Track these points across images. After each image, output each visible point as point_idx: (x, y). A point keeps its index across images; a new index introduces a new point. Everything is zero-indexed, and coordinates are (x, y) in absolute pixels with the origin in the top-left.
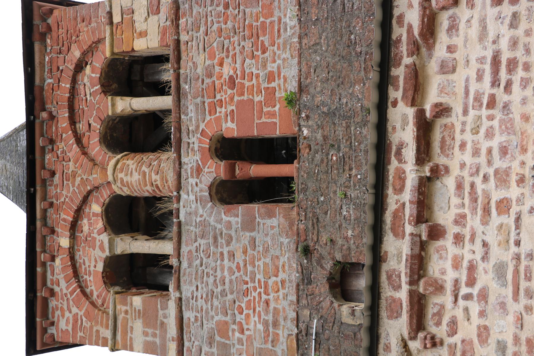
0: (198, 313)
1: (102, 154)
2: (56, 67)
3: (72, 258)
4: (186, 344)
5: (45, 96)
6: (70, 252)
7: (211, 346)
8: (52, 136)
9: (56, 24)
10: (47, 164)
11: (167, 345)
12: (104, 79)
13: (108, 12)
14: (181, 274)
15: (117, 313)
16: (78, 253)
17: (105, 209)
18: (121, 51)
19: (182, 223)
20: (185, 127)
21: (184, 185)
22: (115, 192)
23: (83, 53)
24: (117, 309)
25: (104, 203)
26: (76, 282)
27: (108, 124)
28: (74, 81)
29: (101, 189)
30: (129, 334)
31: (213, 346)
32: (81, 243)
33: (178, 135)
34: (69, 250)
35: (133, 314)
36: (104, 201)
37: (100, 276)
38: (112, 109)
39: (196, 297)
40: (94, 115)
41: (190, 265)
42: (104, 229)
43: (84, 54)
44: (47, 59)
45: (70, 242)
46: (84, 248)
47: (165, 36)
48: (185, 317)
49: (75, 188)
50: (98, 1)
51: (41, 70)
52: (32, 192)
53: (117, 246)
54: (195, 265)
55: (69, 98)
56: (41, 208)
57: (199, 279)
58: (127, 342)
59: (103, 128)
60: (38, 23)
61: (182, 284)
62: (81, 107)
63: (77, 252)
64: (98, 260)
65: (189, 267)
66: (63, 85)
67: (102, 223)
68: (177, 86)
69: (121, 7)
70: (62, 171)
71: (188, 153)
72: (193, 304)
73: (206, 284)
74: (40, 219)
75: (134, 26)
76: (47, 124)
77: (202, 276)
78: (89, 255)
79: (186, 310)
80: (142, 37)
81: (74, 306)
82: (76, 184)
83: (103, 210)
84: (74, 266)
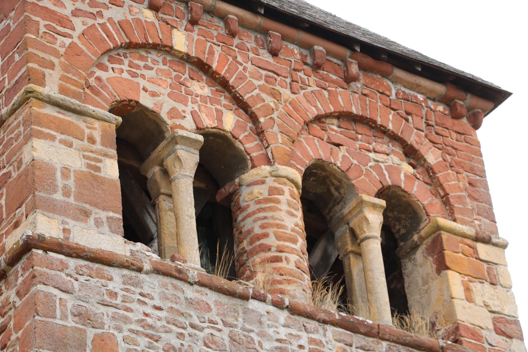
0: (123, 301)
1: (304, 160)
2: (411, 111)
3: (155, 47)
4: (72, 262)
5: (375, 76)
6: (166, 46)
7: (75, 316)
8: (323, 70)
9: (462, 132)
10: (286, 46)
11: (56, 216)
12: (394, 192)
13: (491, 238)
14: (176, 282)
15: (88, 119)
16: (160, 60)
17: (226, 136)
18: (445, 247)
19: (245, 301)
20: (372, 345)
21: (296, 320)
22: (253, 167)
23: (431, 169)
24: (93, 120)
25: (236, 139)
26: (122, 44)
27: (335, 177)
28: (394, 138)
29: (256, 140)
30: (59, 136)
31: (76, 319)
32: (175, 71)
33: (362, 330)
34: (169, 47)
35: (91, 155)
36: (240, 141)
37: (132, 96)
38: (370, 202)
39: (145, 303)
40: (352, 160)
41: (190, 302)
42: (202, 127)
43: (430, 171)
44: (421, 97)
45: (181, 52)
46: (169, 75)
47: (470, 335)
48: (114, 272)
49: (257, 91)
50: (497, 220)
51: (409, 83)
52: (259, 10)
53: (189, 151)
54: (192, 313)
55: (375, 122)
56: (230, 13)
57: (171, 316)
58: (46, 128)
59: (335, 170)
60: (466, 101)
61: (160, 277)
62: (360, 136)
63: (162, 57)
64: (156, 99)
65: (186, 299)
66: (391, 117)
67: (209, 126)
68: (423, 347)
69: (496, 264)
70: (279, 73)
71: (339, 341)
72: (134, 293)
73: (168, 329)
74: (214, 6)
75: (477, 280)
76: (339, 65)
77: (179, 325)
78: (160, 82)
79: (123, 276)
80: (465, 290)
81: (85, 27)
82: (264, 96)
83: (226, 134)
84: (146, 46)
